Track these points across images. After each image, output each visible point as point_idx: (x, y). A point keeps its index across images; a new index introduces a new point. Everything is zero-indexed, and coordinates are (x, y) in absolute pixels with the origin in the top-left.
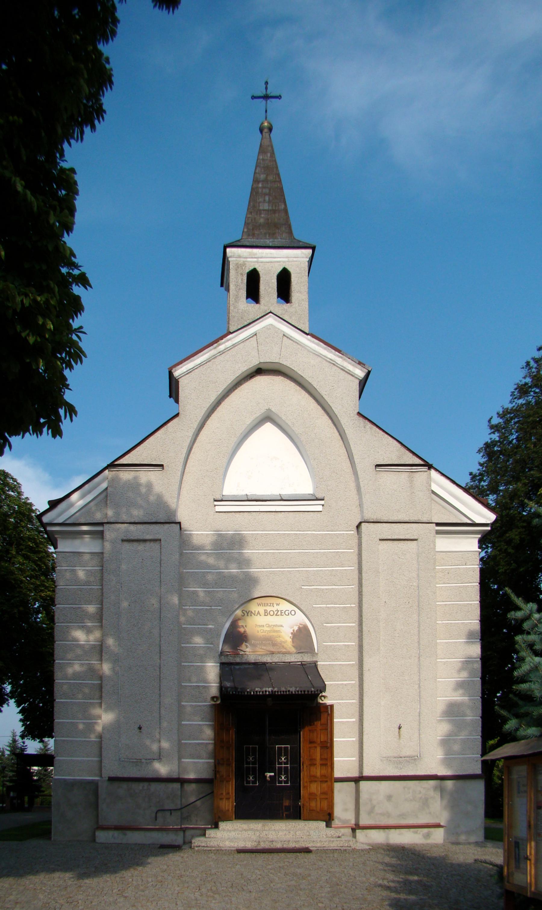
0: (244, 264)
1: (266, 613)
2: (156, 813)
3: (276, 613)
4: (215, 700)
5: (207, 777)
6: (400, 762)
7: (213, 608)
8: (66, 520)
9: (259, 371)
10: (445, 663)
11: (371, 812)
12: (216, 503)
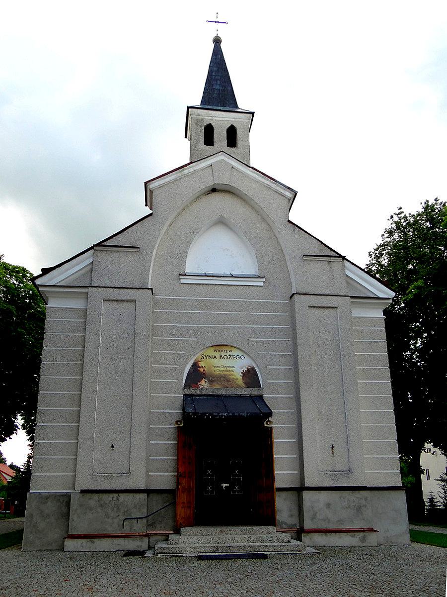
0: (202, 120)
2: (124, 522)
3: (229, 357)
4: (179, 423)
5: (171, 488)
7: (178, 352)
9: (214, 190)
10: (364, 398)
11: (314, 518)
12: (180, 277)
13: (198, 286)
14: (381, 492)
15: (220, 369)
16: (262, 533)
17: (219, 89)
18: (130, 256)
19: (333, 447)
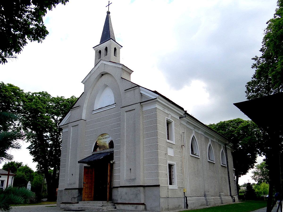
1: (103, 139)
6: (130, 181)
8: (64, 124)
9: (102, 75)
12: (92, 112)
13: (97, 114)
14: (150, 187)
15: (103, 143)
16: (98, 204)
17: (107, 34)
18: (78, 109)
19: (130, 169)
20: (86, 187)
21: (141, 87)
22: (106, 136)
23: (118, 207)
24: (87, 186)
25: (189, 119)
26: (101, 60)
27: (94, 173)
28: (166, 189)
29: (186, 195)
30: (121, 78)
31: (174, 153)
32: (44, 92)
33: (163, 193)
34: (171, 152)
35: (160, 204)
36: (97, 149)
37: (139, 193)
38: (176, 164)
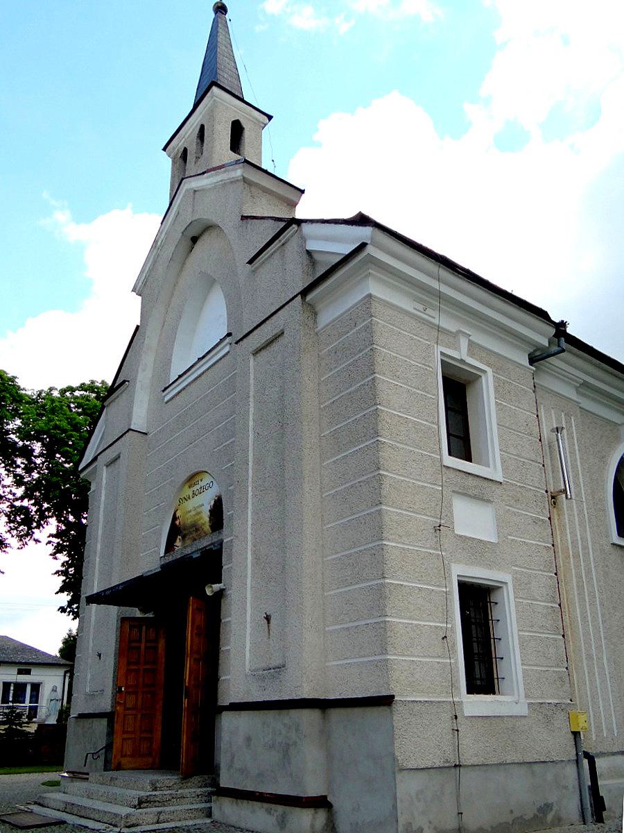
9: (194, 240)
14: (349, 710)
19: (268, 618)
20: (128, 709)
21: (312, 221)
22: (202, 484)
23: (227, 810)
24: (131, 701)
25: (590, 368)
26: (183, 179)
27: (162, 644)
28: (447, 717)
29: (585, 747)
30: (244, 218)
31: (501, 523)
32: (97, 384)
33: (417, 740)
34: (473, 520)
35: (395, 807)
36: (175, 541)
37: (295, 743)
38: (515, 579)
